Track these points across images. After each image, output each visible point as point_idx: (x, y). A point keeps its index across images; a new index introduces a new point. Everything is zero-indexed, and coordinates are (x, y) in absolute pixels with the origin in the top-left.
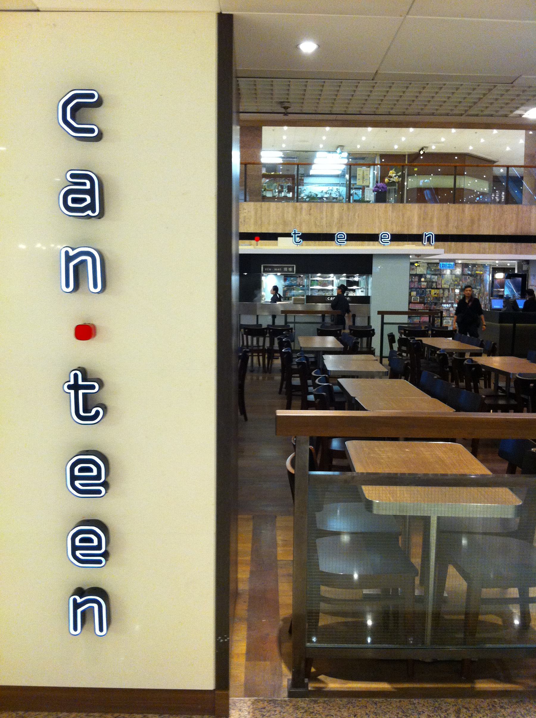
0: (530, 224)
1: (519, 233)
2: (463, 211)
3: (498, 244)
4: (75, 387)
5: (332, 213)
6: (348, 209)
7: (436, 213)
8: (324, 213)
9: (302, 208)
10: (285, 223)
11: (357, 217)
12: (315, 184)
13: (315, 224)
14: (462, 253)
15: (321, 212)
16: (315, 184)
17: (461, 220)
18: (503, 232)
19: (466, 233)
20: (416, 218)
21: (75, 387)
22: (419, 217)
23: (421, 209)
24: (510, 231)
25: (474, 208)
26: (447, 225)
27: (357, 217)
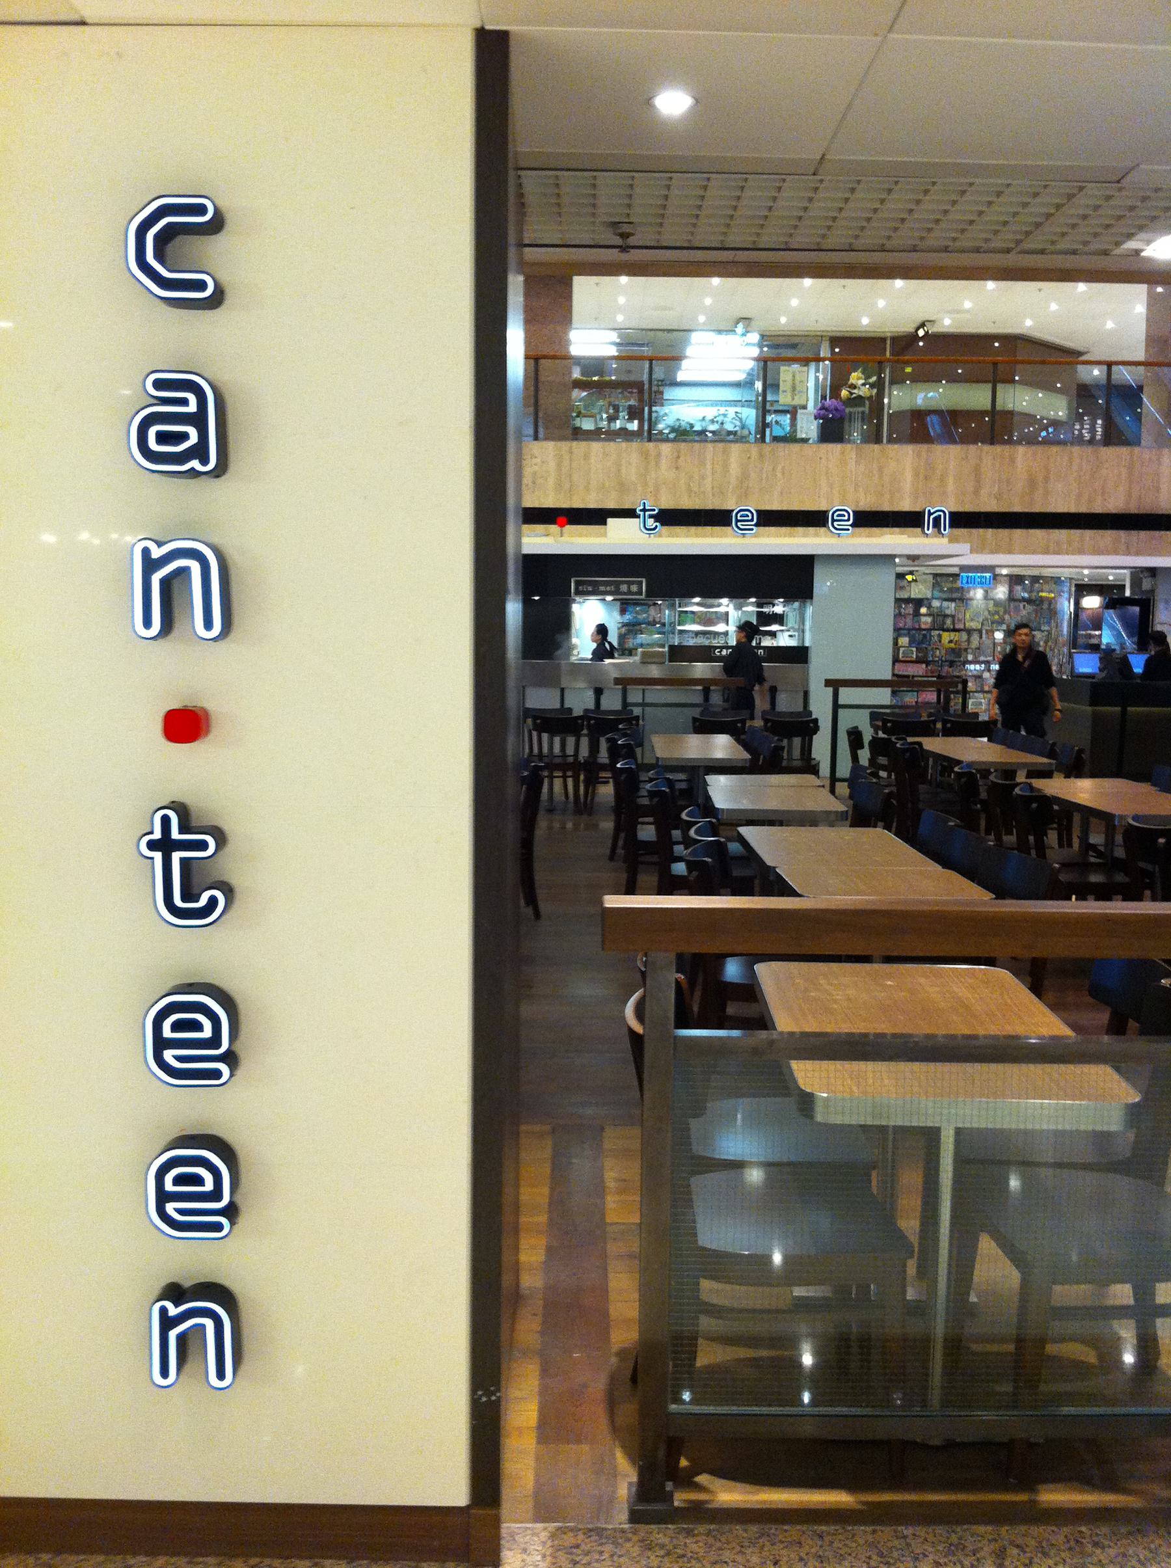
0: (1158, 490)
1: (1133, 509)
2: (1013, 461)
3: (1088, 534)
4: (165, 845)
5: (726, 466)
6: (761, 456)
7: (952, 464)
8: (709, 466)
9: (659, 455)
10: (623, 488)
11: (779, 475)
12: (689, 401)
13: (689, 490)
14: (1010, 552)
15: (702, 463)
16: (689, 401)
17: (1008, 481)
18: (1098, 508)
19: (1017, 508)
20: (908, 476)
21: (165, 845)
22: (916, 474)
23: (919, 456)
24: (1114, 504)
25: (1034, 454)
26: (976, 492)
27: (779, 475)
